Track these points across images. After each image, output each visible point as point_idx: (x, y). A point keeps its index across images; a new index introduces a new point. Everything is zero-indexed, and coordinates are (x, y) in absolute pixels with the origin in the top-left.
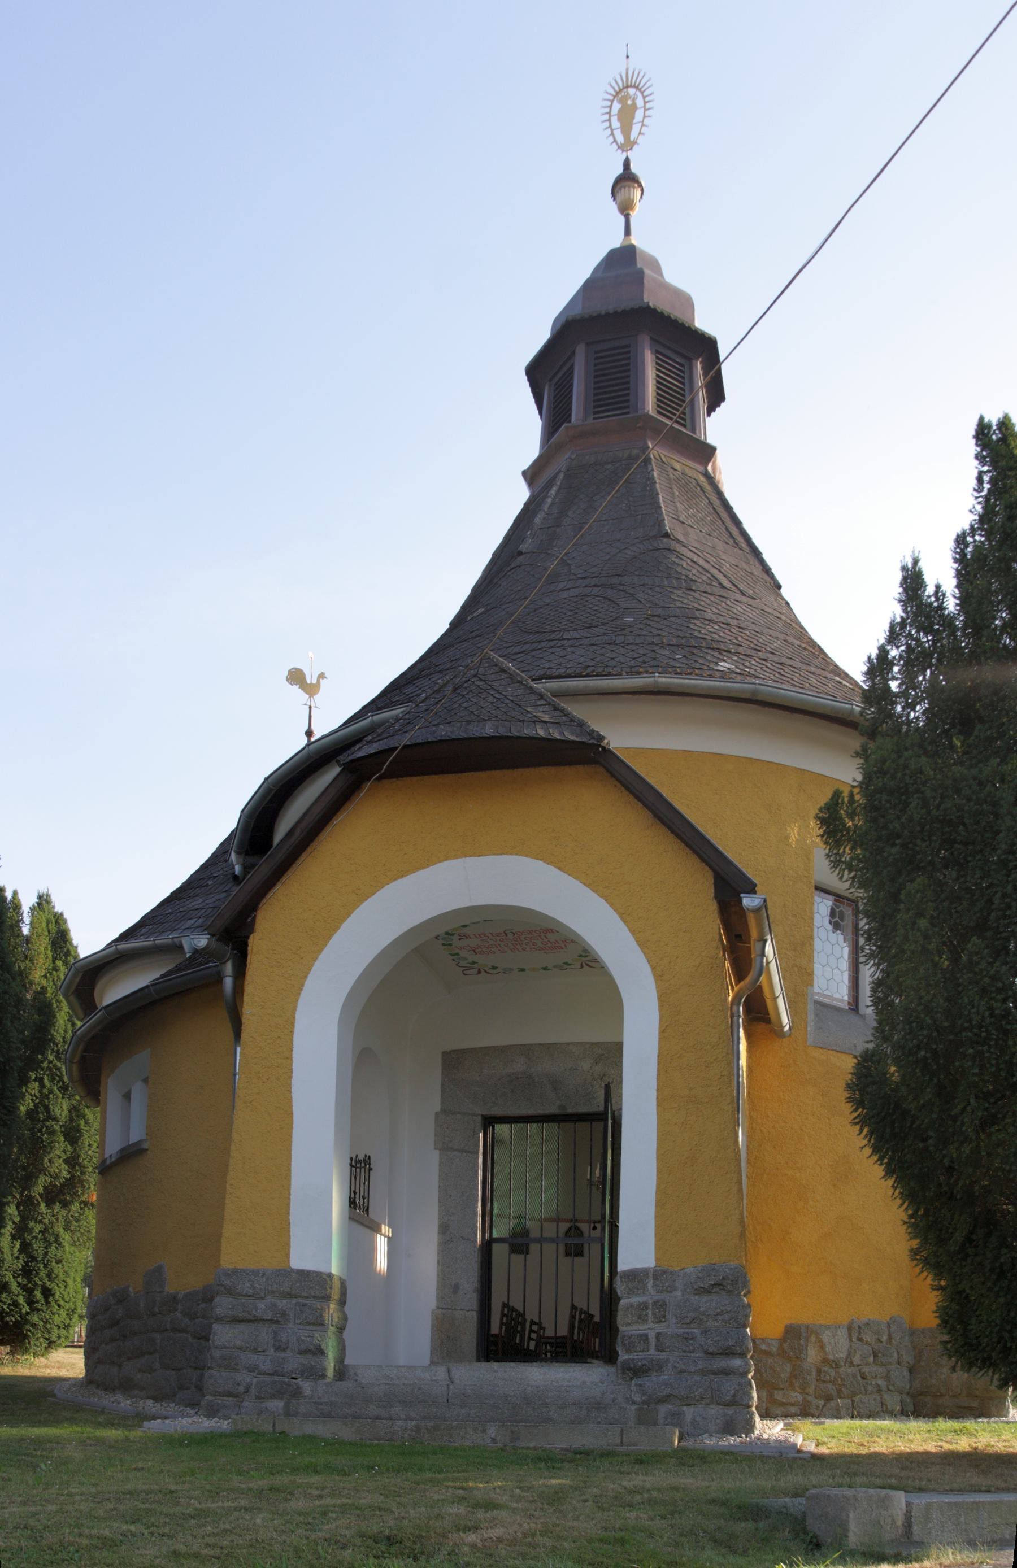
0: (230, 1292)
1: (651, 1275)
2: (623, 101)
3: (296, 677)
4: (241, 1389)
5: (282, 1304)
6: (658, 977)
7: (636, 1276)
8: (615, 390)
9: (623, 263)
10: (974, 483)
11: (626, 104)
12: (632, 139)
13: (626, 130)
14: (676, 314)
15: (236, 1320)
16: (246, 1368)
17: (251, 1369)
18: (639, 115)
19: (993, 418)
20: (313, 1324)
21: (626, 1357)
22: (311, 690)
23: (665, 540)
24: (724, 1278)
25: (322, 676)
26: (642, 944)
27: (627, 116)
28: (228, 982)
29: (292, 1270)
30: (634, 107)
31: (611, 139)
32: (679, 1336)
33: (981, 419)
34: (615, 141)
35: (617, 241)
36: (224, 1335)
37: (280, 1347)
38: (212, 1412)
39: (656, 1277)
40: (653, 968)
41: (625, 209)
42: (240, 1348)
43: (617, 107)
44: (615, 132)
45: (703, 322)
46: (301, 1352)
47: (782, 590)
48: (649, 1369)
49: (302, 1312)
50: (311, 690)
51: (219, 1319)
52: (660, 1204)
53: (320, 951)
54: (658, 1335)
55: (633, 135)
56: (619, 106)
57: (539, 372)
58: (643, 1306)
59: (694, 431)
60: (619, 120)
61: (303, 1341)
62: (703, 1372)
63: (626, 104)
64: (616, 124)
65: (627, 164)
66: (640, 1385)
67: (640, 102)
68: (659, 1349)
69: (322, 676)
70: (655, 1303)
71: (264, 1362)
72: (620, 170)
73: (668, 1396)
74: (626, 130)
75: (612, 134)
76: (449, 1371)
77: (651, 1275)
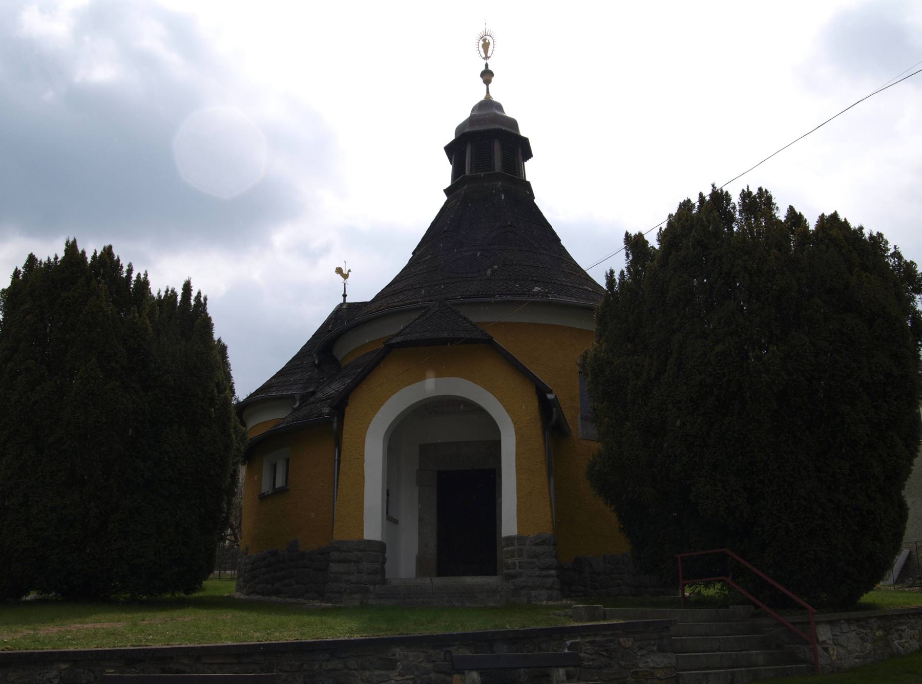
2: (485, 40)
3: (339, 271)
7: (510, 539)
8: (483, 160)
13: (486, 52)
15: (339, 561)
18: (491, 47)
19: (633, 232)
22: (346, 276)
26: (508, 411)
27: (486, 46)
28: (335, 425)
30: (489, 43)
35: (481, 97)
36: (335, 568)
41: (487, 82)
43: (481, 43)
46: (369, 574)
50: (346, 276)
57: (451, 150)
64: (482, 50)
65: (487, 65)
67: (491, 42)
72: (484, 68)
74: (486, 52)
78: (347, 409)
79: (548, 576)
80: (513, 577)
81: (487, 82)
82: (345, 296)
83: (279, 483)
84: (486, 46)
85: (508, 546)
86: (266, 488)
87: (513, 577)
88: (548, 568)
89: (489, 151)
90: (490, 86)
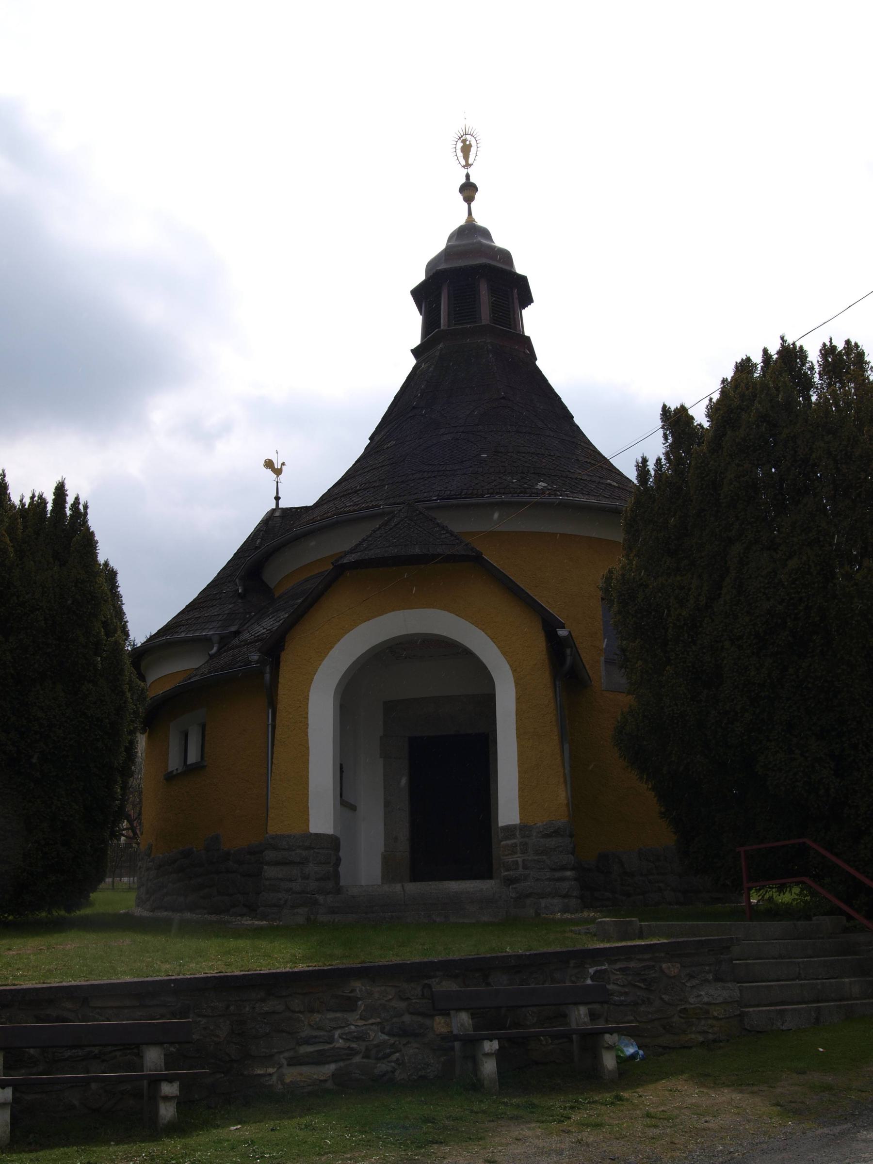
2: (464, 141)
3: (269, 464)
6: (514, 671)
7: (510, 830)
8: (464, 306)
9: (470, 235)
10: (662, 440)
13: (466, 156)
15: (277, 863)
22: (278, 472)
25: (283, 464)
26: (505, 654)
27: (466, 150)
28: (267, 677)
29: (311, 834)
30: (470, 146)
33: (664, 406)
35: (461, 220)
36: (270, 872)
38: (264, 917)
40: (511, 666)
41: (469, 200)
43: (460, 145)
50: (278, 472)
52: (521, 789)
53: (323, 660)
54: (524, 860)
64: (460, 154)
65: (468, 176)
67: (473, 143)
68: (525, 867)
72: (464, 180)
74: (466, 156)
76: (403, 886)
81: (469, 200)
82: (277, 498)
84: (466, 150)
88: (563, 868)
90: (473, 204)
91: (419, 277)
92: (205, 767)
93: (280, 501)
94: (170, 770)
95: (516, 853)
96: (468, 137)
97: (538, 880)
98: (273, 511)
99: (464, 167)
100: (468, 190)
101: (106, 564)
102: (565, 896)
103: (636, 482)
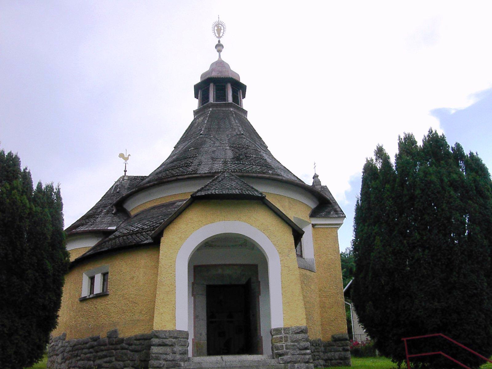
0: (157, 337)
1: (283, 329)
2: (218, 27)
3: (122, 156)
4: (162, 365)
5: (174, 340)
8: (221, 95)
11: (219, 28)
12: (220, 36)
13: (219, 34)
14: (237, 79)
15: (160, 345)
16: (163, 359)
17: (166, 360)
18: (222, 31)
20: (183, 346)
21: (276, 351)
22: (126, 159)
23: (242, 135)
24: (303, 329)
25: (129, 155)
27: (219, 31)
31: (215, 35)
32: (292, 345)
34: (216, 35)
35: (216, 59)
37: (174, 353)
39: (284, 330)
41: (219, 51)
42: (161, 354)
43: (216, 28)
44: (216, 34)
45: (242, 81)
46: (180, 354)
47: (268, 148)
48: (284, 354)
49: (180, 342)
51: (154, 345)
54: (286, 345)
55: (221, 35)
56: (217, 28)
58: (281, 338)
59: (241, 106)
60: (217, 31)
61: (181, 351)
62: (299, 354)
63: (219, 28)
65: (219, 41)
66: (282, 359)
67: (222, 28)
68: (287, 349)
69: (129, 155)
70: (285, 336)
71: (169, 357)
72: (217, 43)
73: (290, 361)
74: (219, 34)
75: (215, 34)
76: (222, 357)
77: (283, 329)
78: (163, 240)
79: (305, 354)
80: (281, 355)
81: (219, 51)
82: (125, 171)
83: (98, 289)
84: (219, 31)
85: (277, 334)
86: (85, 293)
87: (281, 355)
88: (306, 349)
89: (220, 92)
90: (221, 53)
91: (198, 80)
92: (108, 295)
93: (126, 172)
94: (83, 296)
95: (282, 341)
96: (220, 26)
97: (293, 355)
98: (124, 176)
99: (217, 37)
100: (219, 47)
101: (471, 154)
102: (307, 362)
103: (394, 168)
